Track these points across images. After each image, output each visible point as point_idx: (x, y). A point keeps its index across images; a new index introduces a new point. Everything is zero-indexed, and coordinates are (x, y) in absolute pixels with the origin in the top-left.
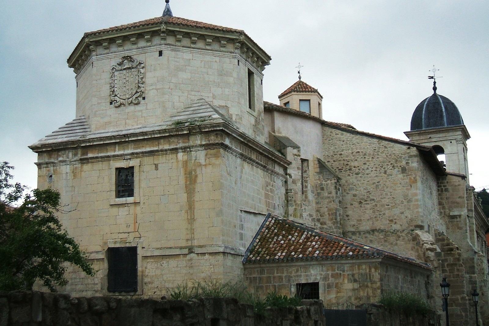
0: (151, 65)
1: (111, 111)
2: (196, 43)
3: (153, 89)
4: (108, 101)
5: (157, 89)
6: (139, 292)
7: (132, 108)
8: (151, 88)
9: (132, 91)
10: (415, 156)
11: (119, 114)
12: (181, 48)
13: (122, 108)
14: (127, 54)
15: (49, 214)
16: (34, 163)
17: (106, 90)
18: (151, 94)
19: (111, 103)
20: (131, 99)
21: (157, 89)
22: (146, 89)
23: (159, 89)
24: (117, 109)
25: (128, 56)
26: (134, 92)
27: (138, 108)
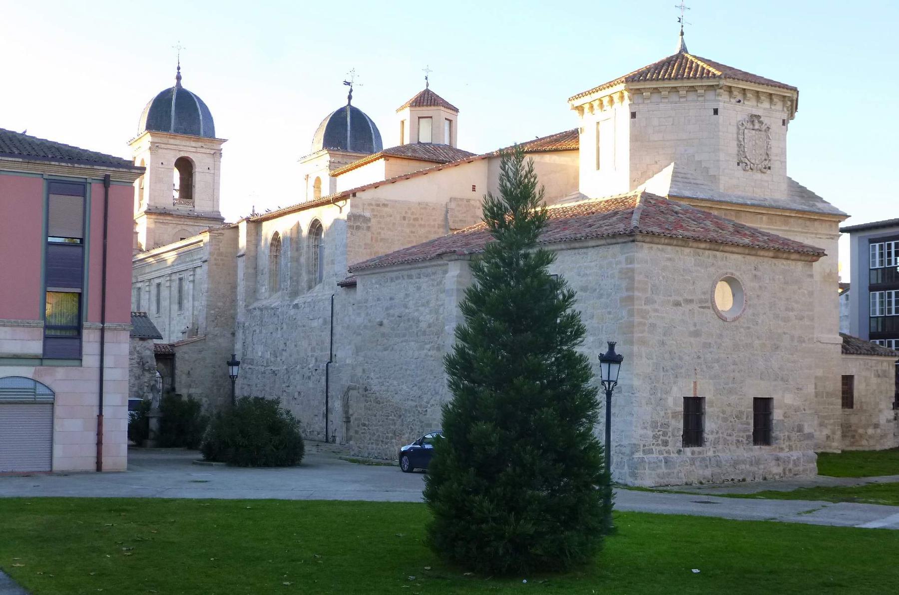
1: (739, 172)
4: (736, 161)
7: (759, 176)
17: (733, 148)
19: (738, 164)
27: (764, 177)
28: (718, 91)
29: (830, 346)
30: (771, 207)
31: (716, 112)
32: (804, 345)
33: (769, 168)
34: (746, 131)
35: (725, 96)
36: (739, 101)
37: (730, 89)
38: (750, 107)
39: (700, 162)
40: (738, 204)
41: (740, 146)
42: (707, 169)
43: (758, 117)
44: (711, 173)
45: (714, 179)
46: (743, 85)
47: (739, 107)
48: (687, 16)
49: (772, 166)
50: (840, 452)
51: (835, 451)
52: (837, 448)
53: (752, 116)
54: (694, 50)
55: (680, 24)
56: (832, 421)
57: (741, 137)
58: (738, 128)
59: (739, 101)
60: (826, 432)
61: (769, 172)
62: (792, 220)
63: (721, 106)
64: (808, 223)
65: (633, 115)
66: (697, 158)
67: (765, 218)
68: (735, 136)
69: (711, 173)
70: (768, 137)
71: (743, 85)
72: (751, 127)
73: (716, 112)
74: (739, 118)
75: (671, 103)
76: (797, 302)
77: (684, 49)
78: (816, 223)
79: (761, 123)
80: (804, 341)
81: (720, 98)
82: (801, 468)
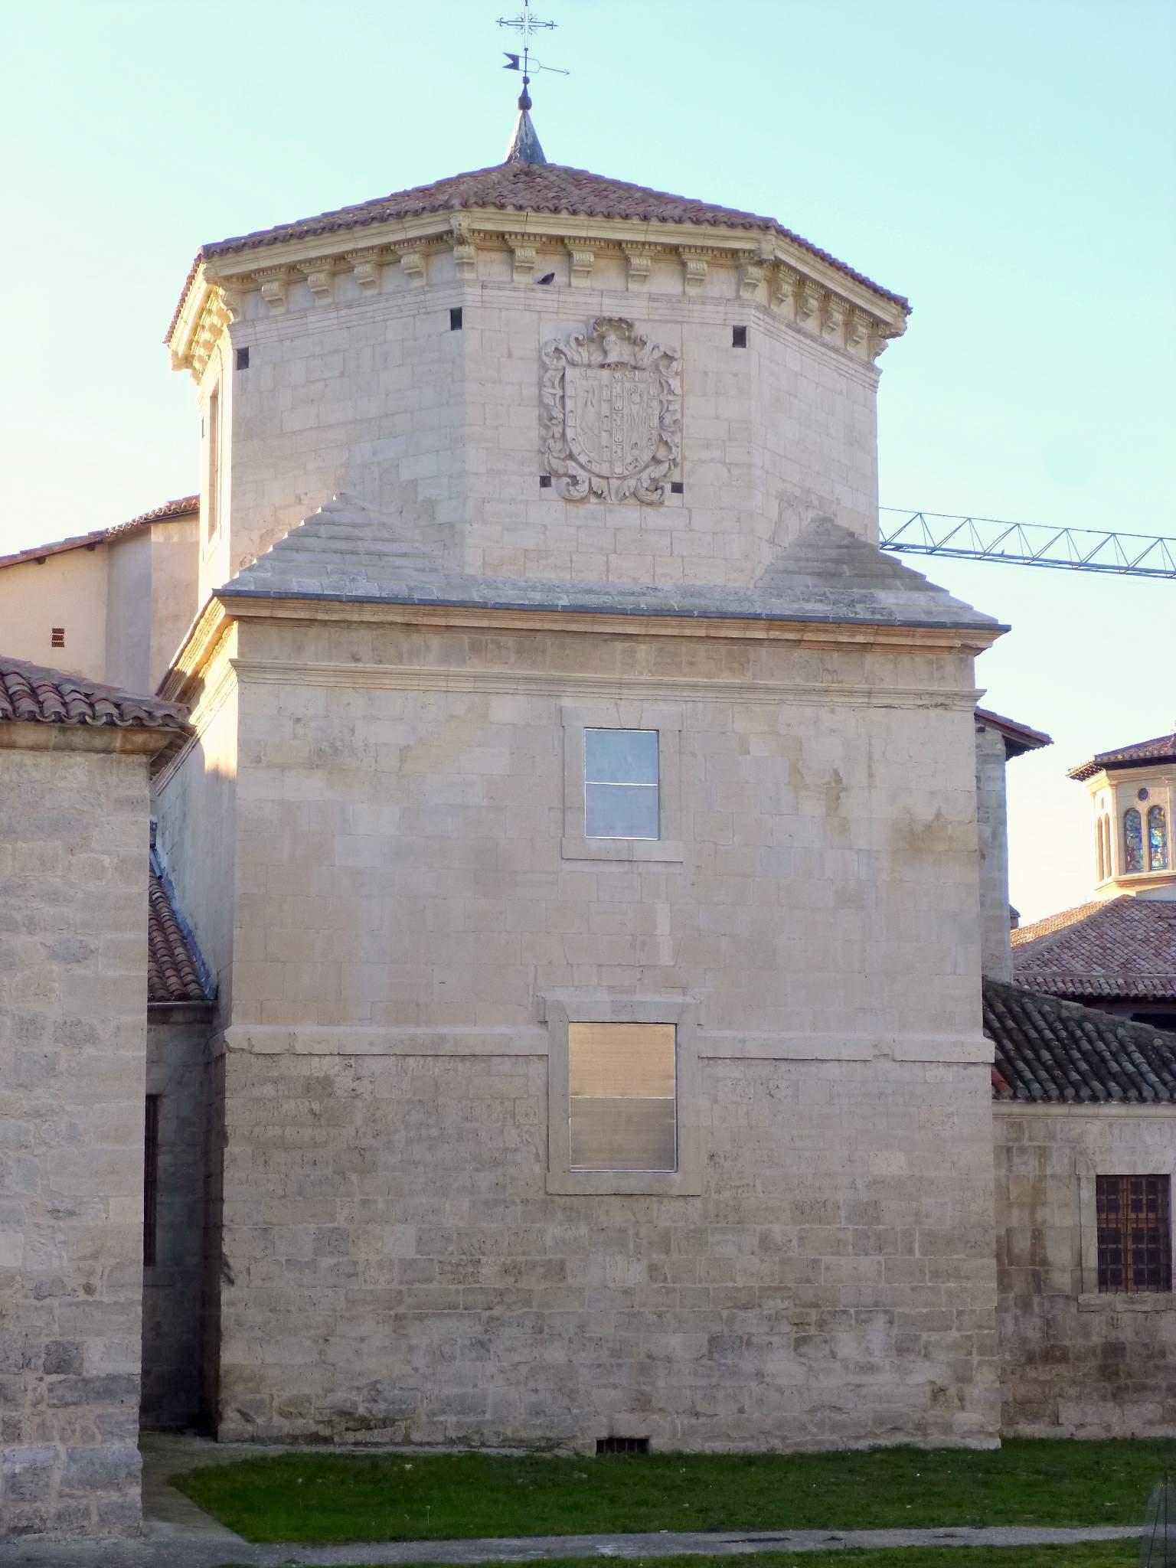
0: (706, 373)
1: (548, 508)
2: (702, 280)
3: (712, 460)
4: (535, 473)
5: (729, 466)
6: (231, 1423)
7: (630, 515)
8: (706, 455)
9: (636, 452)
10: (107, 1388)
11: (579, 528)
12: (784, 328)
13: (589, 506)
14: (612, 309)
15: (155, 934)
16: (1006, 629)
17: (523, 430)
18: (705, 477)
19: (545, 482)
20: (632, 482)
21: (729, 466)
22: (687, 454)
23: (737, 465)
24: (570, 507)
25: (621, 320)
26: (646, 457)
27: (655, 518)
28: (461, 250)
29: (941, 1071)
30: (662, 614)
31: (456, 319)
32: (89, 1051)
33: (677, 488)
34: (570, 373)
35: (492, 265)
36: (547, 280)
37: (502, 242)
38: (597, 292)
39: (414, 483)
40: (523, 609)
41: (547, 420)
42: (431, 506)
43: (623, 325)
44: (443, 515)
45: (450, 534)
46: (670, 234)
47: (543, 297)
48: (540, 47)
49: (686, 482)
50: (995, 1443)
51: (974, 1443)
52: (982, 1431)
53: (600, 322)
54: (557, 153)
55: (519, 75)
56: (954, 1334)
57: (550, 395)
58: (544, 367)
59: (547, 280)
60: (925, 1373)
61: (672, 499)
62: (764, 652)
63: (470, 299)
64: (835, 659)
65: (243, 358)
66: (405, 475)
67: (643, 650)
68: (535, 391)
69: (443, 515)
70: (663, 385)
71: (670, 234)
72: (598, 358)
73: (456, 319)
74: (549, 332)
75: (336, 306)
76: (53, 897)
77: (528, 149)
78: (869, 659)
79: (639, 342)
80: (92, 1038)
81: (468, 275)
82: (51, 1507)
